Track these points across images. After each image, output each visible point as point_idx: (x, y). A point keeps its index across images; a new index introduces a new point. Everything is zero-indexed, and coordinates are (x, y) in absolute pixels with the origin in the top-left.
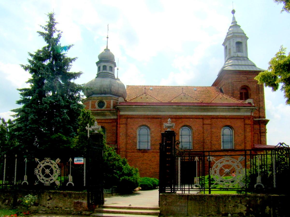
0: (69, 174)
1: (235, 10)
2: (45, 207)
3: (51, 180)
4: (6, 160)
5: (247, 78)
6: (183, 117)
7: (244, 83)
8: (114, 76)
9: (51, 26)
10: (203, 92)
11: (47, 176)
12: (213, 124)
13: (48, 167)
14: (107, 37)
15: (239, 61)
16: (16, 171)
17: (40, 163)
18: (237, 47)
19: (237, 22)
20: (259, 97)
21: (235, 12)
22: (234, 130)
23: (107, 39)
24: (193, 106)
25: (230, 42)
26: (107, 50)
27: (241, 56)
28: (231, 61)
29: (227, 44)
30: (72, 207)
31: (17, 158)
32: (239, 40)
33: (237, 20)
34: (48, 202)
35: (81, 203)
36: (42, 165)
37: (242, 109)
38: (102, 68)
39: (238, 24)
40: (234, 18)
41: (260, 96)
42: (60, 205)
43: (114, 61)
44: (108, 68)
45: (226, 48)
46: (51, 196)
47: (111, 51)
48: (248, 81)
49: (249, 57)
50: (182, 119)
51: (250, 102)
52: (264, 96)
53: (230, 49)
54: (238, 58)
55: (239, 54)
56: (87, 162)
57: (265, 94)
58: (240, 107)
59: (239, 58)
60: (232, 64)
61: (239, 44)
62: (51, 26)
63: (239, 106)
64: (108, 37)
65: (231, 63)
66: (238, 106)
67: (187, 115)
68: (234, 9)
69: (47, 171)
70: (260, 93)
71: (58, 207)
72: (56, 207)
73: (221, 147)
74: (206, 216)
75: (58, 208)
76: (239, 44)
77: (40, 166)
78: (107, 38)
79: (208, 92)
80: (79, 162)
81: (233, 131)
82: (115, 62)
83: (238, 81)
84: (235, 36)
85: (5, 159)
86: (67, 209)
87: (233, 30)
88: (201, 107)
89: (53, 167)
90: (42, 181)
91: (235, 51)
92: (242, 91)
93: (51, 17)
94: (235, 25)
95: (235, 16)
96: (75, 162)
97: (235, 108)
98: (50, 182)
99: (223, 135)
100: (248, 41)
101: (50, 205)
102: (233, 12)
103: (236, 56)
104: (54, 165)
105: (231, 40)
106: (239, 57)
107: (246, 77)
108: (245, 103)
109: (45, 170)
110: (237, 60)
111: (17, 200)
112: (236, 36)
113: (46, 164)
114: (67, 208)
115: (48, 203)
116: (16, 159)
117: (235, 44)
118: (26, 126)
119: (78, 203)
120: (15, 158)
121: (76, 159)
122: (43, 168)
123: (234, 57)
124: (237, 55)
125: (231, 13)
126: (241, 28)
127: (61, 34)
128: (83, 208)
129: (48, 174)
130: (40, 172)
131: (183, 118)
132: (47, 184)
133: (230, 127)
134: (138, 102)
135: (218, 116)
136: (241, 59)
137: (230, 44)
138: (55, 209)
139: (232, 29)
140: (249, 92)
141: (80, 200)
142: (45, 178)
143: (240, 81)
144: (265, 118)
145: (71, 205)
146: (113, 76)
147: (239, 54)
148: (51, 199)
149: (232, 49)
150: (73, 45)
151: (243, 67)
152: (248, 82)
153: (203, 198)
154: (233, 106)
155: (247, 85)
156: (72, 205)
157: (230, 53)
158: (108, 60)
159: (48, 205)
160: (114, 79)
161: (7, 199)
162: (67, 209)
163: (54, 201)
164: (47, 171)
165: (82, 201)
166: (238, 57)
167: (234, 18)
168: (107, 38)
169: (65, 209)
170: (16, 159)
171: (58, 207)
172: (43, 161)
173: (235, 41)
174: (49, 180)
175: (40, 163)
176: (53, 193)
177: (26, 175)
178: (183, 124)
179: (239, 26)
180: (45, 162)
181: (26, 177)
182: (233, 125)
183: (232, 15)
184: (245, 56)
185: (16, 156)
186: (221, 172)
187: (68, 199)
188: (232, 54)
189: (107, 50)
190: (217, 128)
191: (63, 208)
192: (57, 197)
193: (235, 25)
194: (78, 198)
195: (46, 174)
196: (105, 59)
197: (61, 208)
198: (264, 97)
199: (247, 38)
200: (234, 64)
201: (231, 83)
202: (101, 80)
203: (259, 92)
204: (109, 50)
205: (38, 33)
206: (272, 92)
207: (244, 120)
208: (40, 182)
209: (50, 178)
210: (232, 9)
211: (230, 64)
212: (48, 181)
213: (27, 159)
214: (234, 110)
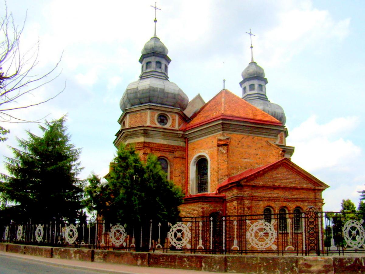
3: (266, 244)
4: (213, 223)
8: (266, 97)
11: (179, 240)
13: (179, 231)
14: (251, 46)
16: (89, 234)
23: (251, 49)
31: (212, 221)
36: (174, 228)
37: (170, 104)
38: (153, 65)
43: (264, 76)
64: (252, 46)
69: (179, 235)
77: (173, 230)
82: (265, 77)
85: (212, 222)
89: (184, 230)
90: (171, 229)
98: (264, 247)
104: (185, 229)
109: (177, 234)
113: (178, 228)
116: (151, 224)
120: (210, 221)
129: (180, 238)
130: (173, 235)
134: (173, 141)
144: (151, 112)
146: (264, 97)
160: (266, 101)
164: (179, 235)
168: (155, 21)
170: (151, 224)
172: (175, 225)
174: (264, 245)
175: (172, 227)
180: (117, 227)
185: (151, 221)
186: (179, 240)
195: (178, 238)
198: (140, 59)
204: (255, 63)
205: (41, 131)
209: (265, 242)
212: (179, 244)
213: (170, 223)
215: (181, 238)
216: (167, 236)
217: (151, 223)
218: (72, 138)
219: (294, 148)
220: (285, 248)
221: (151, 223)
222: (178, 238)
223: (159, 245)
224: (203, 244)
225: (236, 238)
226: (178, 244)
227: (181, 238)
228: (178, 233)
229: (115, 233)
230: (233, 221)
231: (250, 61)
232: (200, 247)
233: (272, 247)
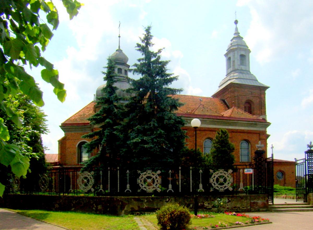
0: (200, 183)
1: (238, 21)
2: (225, 208)
3: (225, 187)
4: (181, 171)
5: (252, 92)
6: (234, 131)
7: (248, 97)
9: (147, 39)
10: (209, 103)
12: (233, 138)
14: (119, 35)
15: (244, 75)
17: (156, 174)
18: (241, 60)
19: (239, 33)
20: (261, 112)
21: (238, 23)
22: (251, 144)
23: (119, 38)
24: (217, 119)
25: (234, 54)
26: (119, 50)
27: (244, 69)
28: (236, 74)
29: (231, 55)
30: (249, 206)
32: (243, 53)
33: (239, 31)
34: (227, 204)
35: (257, 203)
39: (241, 35)
40: (236, 29)
41: (262, 112)
42: (238, 205)
44: (123, 71)
45: (229, 59)
46: (230, 199)
47: (124, 52)
48: (252, 95)
49: (251, 71)
50: (205, 131)
51: (264, 118)
52: (266, 111)
53: (234, 61)
54: (241, 71)
55: (243, 68)
56: (254, 172)
57: (267, 110)
58: (257, 123)
59: (242, 71)
60: (237, 77)
61: (242, 56)
62: (147, 39)
63: (256, 122)
65: (237, 76)
66: (255, 122)
67: (211, 128)
68: (237, 19)
70: (263, 108)
71: (236, 207)
72: (235, 207)
73: (239, 160)
74: (247, 225)
75: (236, 209)
76: (242, 56)
78: (119, 37)
79: (213, 104)
80: (248, 172)
81: (250, 145)
83: (243, 94)
84: (240, 48)
86: (244, 208)
87: (237, 42)
88: (217, 120)
90: (217, 188)
91: (239, 63)
92: (246, 105)
93: (148, 30)
94: (238, 37)
95: (237, 27)
96: (245, 172)
97: (252, 124)
99: (241, 149)
100: (250, 54)
101: (229, 206)
102: (236, 22)
103: (240, 69)
105: (236, 52)
106: (243, 70)
107: (250, 91)
108: (259, 118)
110: (241, 73)
111: (198, 204)
112: (241, 48)
114: (244, 208)
115: (228, 205)
116: (109, 171)
117: (239, 57)
118: (152, 139)
119: (254, 203)
120: (179, 170)
121: (246, 170)
122: (217, 178)
123: (238, 70)
124: (241, 68)
125: (234, 24)
126: (243, 40)
127: (163, 49)
128: (259, 206)
131: (207, 131)
132: (222, 190)
133: (248, 141)
135: (243, 130)
136: (245, 72)
137: (234, 56)
138: (234, 209)
139: (237, 40)
140: (252, 106)
141: (255, 201)
142: (219, 186)
143: (245, 95)
145: (247, 205)
147: (243, 68)
148: (229, 201)
149: (236, 62)
150: (170, 61)
151: (248, 81)
152: (252, 96)
153: (249, 208)
154: (251, 121)
155: (251, 99)
156: (248, 205)
157: (234, 65)
158: (123, 62)
159: (227, 207)
161: (191, 204)
162: (244, 208)
163: (233, 203)
165: (257, 201)
166: (241, 70)
167: (236, 29)
168: (119, 37)
169: (243, 209)
171: (236, 207)
172: (217, 172)
173: (239, 54)
176: (232, 197)
177: (202, 183)
178: (207, 136)
179: (242, 38)
181: (201, 186)
182: (250, 140)
183: (235, 25)
184: (247, 70)
187: (244, 200)
188: (236, 67)
189: (119, 50)
190: (236, 142)
191: (241, 208)
192: (235, 199)
193: (238, 37)
194: (254, 200)
196: (119, 61)
197: (239, 208)
199: (249, 51)
200: (239, 77)
201: (237, 96)
202: (120, 84)
203: (261, 107)
204: (121, 51)
206: (36, 68)
207: (259, 135)
208: (215, 189)
210: (235, 20)
211: (236, 77)
214: (251, 125)
215: (87, 183)
216: (162, 180)
217: (109, 170)
218: (153, 38)
219: (271, 123)
220: (238, 189)
221: (109, 170)
222: (224, 181)
223: (101, 189)
224: (203, 188)
225: (241, 182)
226: (221, 188)
227: (87, 183)
228: (148, 179)
229: (83, 180)
230: (240, 169)
231: (117, 49)
232: (241, 189)
233: (229, 189)
